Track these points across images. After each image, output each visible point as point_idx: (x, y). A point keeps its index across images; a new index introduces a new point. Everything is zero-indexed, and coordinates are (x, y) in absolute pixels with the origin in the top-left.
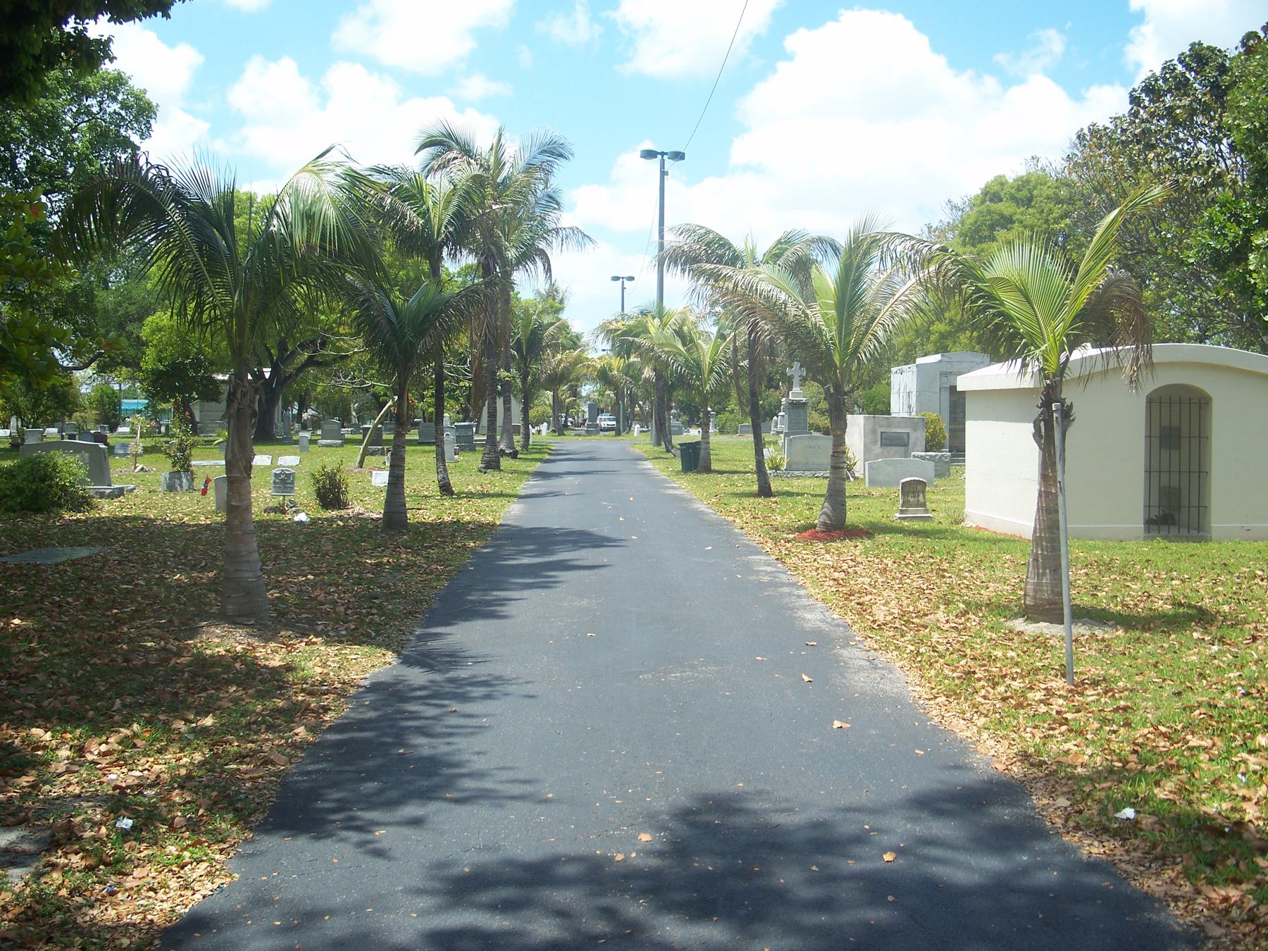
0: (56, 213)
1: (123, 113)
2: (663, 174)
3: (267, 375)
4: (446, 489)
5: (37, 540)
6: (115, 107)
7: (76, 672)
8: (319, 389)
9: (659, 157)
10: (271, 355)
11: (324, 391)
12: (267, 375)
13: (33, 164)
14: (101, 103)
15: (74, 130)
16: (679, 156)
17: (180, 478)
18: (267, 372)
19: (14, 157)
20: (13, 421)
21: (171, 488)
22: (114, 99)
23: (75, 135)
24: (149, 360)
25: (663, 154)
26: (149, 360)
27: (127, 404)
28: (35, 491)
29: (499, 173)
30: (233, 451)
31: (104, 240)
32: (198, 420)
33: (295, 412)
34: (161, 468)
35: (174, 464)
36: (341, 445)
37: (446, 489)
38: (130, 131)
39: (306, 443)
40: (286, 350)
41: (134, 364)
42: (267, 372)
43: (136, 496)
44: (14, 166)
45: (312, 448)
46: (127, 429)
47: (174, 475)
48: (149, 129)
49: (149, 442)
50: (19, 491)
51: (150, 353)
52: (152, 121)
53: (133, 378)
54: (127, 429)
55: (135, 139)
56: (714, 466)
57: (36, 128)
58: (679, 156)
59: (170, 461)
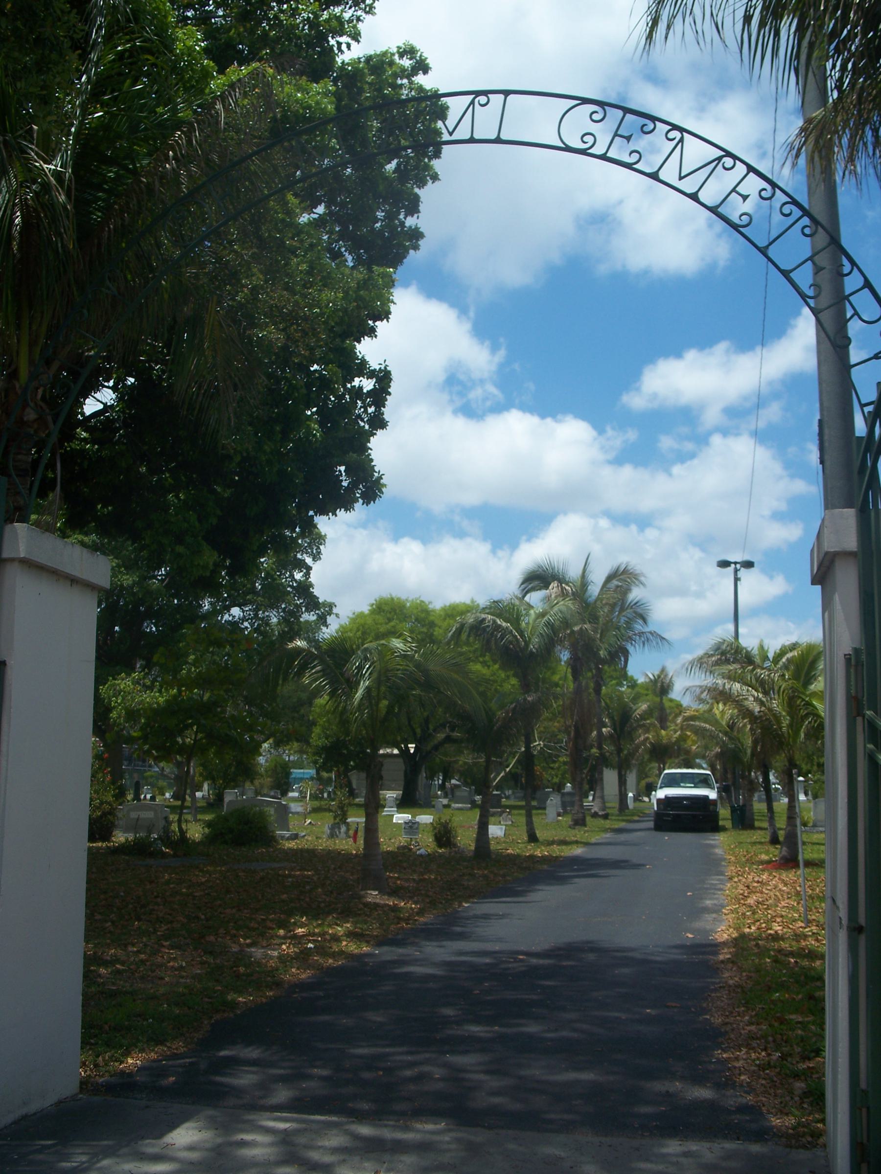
0: (247, 620)
2: (737, 580)
3: (412, 751)
4: (533, 838)
9: (733, 566)
10: (415, 734)
12: (412, 751)
16: (749, 565)
17: (340, 829)
18: (412, 747)
21: (332, 835)
24: (317, 737)
25: (735, 563)
26: (317, 737)
27: (296, 772)
31: (34, 187)
32: (354, 786)
33: (440, 782)
35: (335, 818)
36: (471, 809)
37: (533, 838)
38: (305, 555)
41: (304, 739)
42: (412, 747)
43: (307, 840)
46: (296, 794)
48: (319, 553)
49: (316, 804)
51: (317, 730)
52: (322, 547)
53: (301, 752)
54: (296, 794)
55: (309, 560)
56: (757, 824)
58: (749, 565)
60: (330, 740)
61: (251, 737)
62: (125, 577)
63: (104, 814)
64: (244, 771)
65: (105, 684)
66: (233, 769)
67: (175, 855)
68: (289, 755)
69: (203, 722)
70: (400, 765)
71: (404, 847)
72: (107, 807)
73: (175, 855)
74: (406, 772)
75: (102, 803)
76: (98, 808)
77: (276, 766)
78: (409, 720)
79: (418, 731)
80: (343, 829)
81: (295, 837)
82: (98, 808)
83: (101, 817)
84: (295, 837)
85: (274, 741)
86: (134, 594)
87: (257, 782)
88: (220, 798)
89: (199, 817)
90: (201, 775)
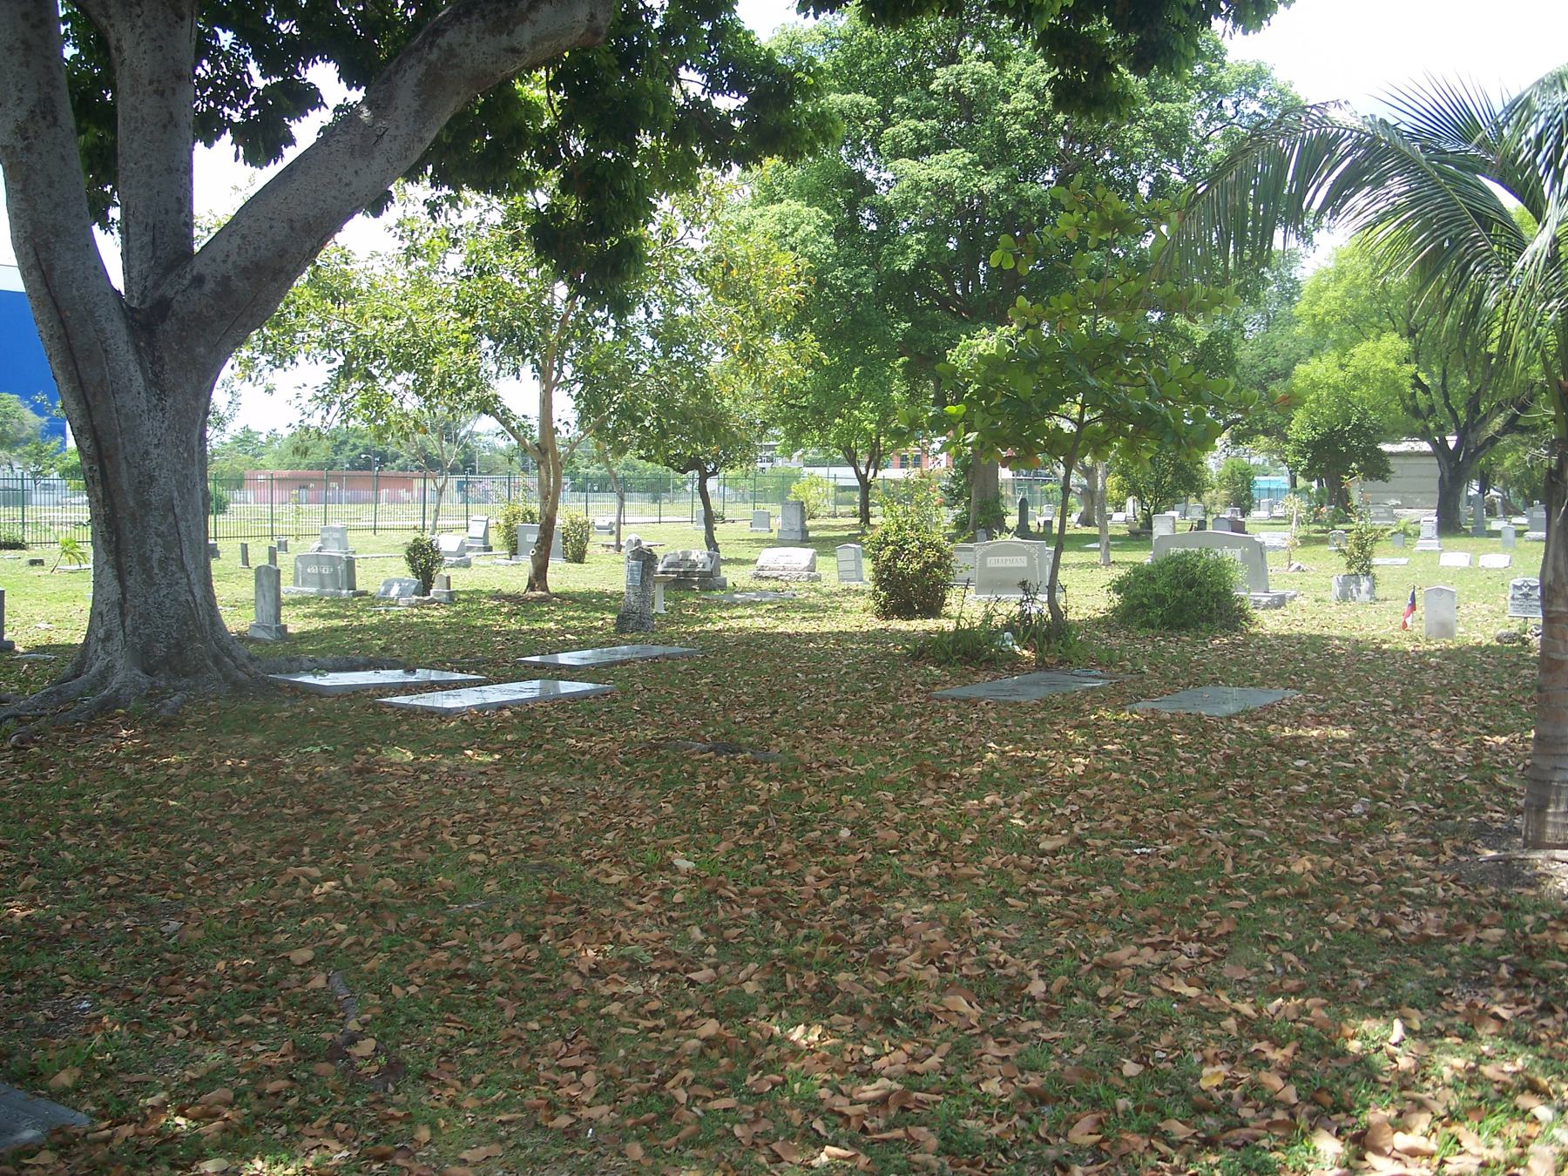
1: (1265, 113)
3: (1451, 445)
5: (1196, 677)
6: (1254, 106)
7: (1311, 942)
8: (1507, 463)
11: (1514, 465)
12: (1451, 445)
13: (1159, 187)
14: (1237, 104)
15: (1205, 141)
17: (1358, 584)
18: (1452, 441)
19: (1135, 180)
20: (1130, 501)
21: (1344, 596)
22: (1253, 97)
23: (1208, 147)
26: (1299, 426)
27: (1261, 482)
28: (1180, 601)
29: (309, 671)
30: (1555, 569)
34: (1328, 565)
35: (1349, 565)
39: (1510, 535)
40: (1478, 411)
41: (1277, 432)
42: (1452, 441)
44: (1135, 190)
45: (1520, 542)
47: (1349, 581)
50: (1160, 600)
51: (1299, 415)
57: (1160, 139)
59: (1344, 560)
60: (1320, 430)
61: (1198, 416)
62: (985, 179)
63: (927, 567)
64: (1188, 482)
65: (955, 346)
66: (1169, 479)
67: (1041, 665)
68: (1256, 455)
69: (1092, 382)
70: (1433, 469)
71: (1512, 638)
72: (931, 556)
73: (1041, 665)
74: (1441, 479)
75: (923, 548)
76: (916, 556)
77: (1233, 473)
78: (1446, 396)
79: (1461, 414)
80: (1365, 584)
81: (1280, 602)
82: (916, 556)
83: (923, 571)
84: (1280, 602)
85: (1231, 436)
86: (1000, 206)
87: (1206, 497)
88: (1148, 524)
89: (1115, 556)
90: (1120, 488)
